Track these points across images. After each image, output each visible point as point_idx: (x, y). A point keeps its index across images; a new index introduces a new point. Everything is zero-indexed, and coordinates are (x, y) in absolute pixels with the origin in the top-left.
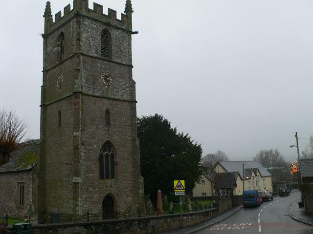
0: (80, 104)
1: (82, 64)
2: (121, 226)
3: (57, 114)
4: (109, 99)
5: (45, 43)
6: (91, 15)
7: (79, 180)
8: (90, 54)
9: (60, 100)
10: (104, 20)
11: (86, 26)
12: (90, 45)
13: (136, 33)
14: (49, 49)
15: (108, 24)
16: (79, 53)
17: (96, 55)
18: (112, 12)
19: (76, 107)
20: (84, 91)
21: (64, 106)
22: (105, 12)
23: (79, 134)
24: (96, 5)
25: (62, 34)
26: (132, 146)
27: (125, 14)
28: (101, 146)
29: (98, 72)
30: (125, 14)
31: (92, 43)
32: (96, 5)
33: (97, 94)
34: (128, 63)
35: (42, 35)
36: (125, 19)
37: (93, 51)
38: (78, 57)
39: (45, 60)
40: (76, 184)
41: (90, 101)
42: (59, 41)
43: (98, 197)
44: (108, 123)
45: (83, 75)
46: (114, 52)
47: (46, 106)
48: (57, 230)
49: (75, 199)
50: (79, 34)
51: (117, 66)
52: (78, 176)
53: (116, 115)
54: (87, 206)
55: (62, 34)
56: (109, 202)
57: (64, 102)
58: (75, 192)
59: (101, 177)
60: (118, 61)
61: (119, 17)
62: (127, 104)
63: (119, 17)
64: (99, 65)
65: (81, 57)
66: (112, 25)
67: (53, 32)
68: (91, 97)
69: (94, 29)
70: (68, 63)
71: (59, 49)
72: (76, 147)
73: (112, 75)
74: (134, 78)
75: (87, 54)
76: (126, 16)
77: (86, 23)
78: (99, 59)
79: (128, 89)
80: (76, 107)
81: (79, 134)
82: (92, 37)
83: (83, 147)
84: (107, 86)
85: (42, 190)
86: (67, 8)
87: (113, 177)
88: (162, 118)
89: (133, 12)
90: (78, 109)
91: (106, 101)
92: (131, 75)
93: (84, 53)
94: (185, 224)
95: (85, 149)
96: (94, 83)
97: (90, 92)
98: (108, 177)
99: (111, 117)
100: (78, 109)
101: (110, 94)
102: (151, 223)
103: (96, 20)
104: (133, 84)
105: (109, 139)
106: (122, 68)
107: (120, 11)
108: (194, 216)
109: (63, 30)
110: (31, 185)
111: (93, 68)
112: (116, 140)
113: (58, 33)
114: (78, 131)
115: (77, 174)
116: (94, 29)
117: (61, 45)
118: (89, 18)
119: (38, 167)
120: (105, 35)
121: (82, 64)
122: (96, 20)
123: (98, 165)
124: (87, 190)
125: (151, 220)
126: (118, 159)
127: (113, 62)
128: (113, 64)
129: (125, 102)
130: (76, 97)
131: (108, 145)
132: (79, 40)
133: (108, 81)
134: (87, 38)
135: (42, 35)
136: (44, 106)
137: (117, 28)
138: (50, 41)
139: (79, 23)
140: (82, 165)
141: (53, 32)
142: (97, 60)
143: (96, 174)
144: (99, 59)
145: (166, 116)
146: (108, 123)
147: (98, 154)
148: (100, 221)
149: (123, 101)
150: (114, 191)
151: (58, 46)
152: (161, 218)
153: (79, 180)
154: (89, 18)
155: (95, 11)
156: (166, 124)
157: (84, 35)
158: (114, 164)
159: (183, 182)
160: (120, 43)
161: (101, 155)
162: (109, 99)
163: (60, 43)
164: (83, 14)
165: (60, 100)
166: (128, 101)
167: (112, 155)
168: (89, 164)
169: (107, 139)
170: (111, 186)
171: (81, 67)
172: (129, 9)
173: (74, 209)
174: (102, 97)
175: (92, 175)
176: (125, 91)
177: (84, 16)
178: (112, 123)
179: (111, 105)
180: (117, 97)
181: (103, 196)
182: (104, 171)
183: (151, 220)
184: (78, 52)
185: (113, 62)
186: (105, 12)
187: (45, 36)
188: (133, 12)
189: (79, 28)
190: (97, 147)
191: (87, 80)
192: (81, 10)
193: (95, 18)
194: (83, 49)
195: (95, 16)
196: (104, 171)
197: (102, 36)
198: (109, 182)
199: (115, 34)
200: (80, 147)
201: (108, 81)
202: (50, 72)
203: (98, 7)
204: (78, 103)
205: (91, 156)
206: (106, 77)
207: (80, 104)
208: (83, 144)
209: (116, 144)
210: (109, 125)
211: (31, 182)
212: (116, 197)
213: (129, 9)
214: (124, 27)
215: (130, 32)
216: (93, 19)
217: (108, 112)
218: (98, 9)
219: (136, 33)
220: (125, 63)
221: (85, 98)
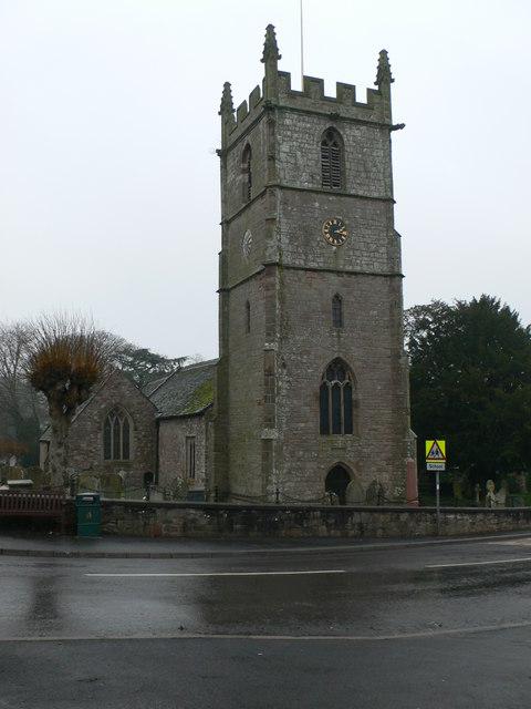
0: (278, 287)
1: (279, 207)
2: (283, 517)
3: (244, 308)
4: (339, 273)
5: (224, 167)
6: (298, 104)
7: (274, 434)
8: (298, 185)
9: (248, 280)
10: (327, 110)
11: (287, 128)
12: (296, 167)
13: (401, 126)
14: (230, 178)
15: (335, 117)
16: (275, 186)
17: (310, 186)
18: (346, 90)
19: (270, 293)
20: (287, 260)
21: (254, 292)
22: (330, 91)
23: (275, 346)
24: (308, 81)
25: (248, 147)
26: (394, 368)
27: (376, 88)
28: (322, 369)
29: (316, 219)
30: (376, 88)
31: (301, 162)
32: (308, 81)
33: (313, 265)
34: (383, 195)
35: (218, 151)
36: (377, 99)
37: (305, 177)
38: (273, 194)
39: (224, 201)
40: (267, 442)
41: (300, 279)
42: (244, 162)
43: (317, 469)
44: (339, 322)
45: (284, 228)
46: (350, 174)
47: (228, 291)
48: (154, 512)
49: (266, 470)
50: (273, 147)
51: (358, 203)
52: (272, 427)
53: (355, 305)
54: (293, 485)
55: (248, 147)
56: (338, 478)
57: (253, 282)
58: (266, 457)
59: (324, 430)
60: (361, 193)
61: (361, 98)
62: (380, 280)
63: (361, 98)
64: (317, 204)
65: (279, 193)
66: (344, 119)
67: (235, 144)
68: (301, 272)
69: (305, 131)
70: (257, 206)
71: (247, 176)
72: (269, 372)
73: (347, 222)
74: (398, 227)
75: (289, 185)
76: (378, 93)
77: (288, 122)
78: (317, 192)
79: (383, 250)
80: (270, 293)
81: (275, 346)
82: (301, 149)
83: (285, 371)
84: (334, 248)
85: (222, 451)
86: (254, 94)
87: (349, 430)
88: (498, 303)
89: (393, 81)
90: (272, 297)
91: (333, 278)
92: (391, 219)
93: (284, 183)
94: (452, 530)
95: (289, 374)
96: (307, 244)
97: (299, 262)
98: (336, 431)
99: (345, 309)
100: (272, 297)
101: (342, 262)
102: (357, 518)
103: (308, 113)
104: (394, 240)
105: (341, 355)
106: (370, 206)
107: (364, 82)
108: (480, 517)
109: (248, 139)
110: (203, 443)
111: (304, 212)
112: (356, 356)
113: (241, 147)
114: (272, 341)
115: (269, 422)
116: (305, 131)
117: (247, 171)
118: (292, 110)
119: (215, 408)
120: (331, 139)
121: (279, 207)
122: (308, 113)
123: (316, 406)
124: (292, 454)
125: (356, 514)
126: (358, 395)
127: (350, 196)
128: (348, 199)
129: (378, 278)
130: (270, 274)
131: (338, 367)
132: (272, 158)
133: (338, 237)
134: (291, 154)
135: (218, 151)
136: (224, 291)
137: (358, 122)
138: (231, 163)
139: (271, 124)
140: (281, 406)
141: (235, 144)
142: (314, 195)
143: (314, 423)
144: (317, 192)
145: (507, 298)
146: (339, 322)
147: (317, 386)
148: (270, 505)
149: (373, 274)
150: (349, 459)
151: (244, 171)
152: (384, 511)
153: (274, 434)
154: (292, 110)
155: (306, 94)
156: (509, 318)
157: (285, 148)
158: (351, 405)
159: (442, 444)
160: (364, 154)
161: (324, 387)
162: (339, 273)
163: (246, 166)
164: (281, 104)
165: (248, 280)
166: (385, 276)
167: (348, 388)
168: (299, 405)
169: (336, 356)
170: (342, 448)
171: (278, 214)
172: (384, 75)
173: (264, 487)
174: (324, 271)
175: (303, 425)
176: (377, 255)
177: (286, 108)
178: (346, 322)
179: (344, 286)
180: (358, 269)
181: (325, 468)
182: (331, 417)
183: (356, 514)
184: (271, 183)
185: (350, 196)
186: (330, 91)
187: (223, 154)
188: (393, 81)
189: (273, 134)
190: (314, 372)
191: (292, 238)
192: (277, 97)
193: (307, 108)
194: (282, 175)
195: (308, 104)
196: (331, 417)
197: (324, 143)
198: (340, 440)
199: (351, 135)
200: (277, 370)
201: (338, 237)
202: (233, 224)
203: (314, 84)
204: (273, 285)
205: (301, 388)
206: (334, 228)
207: (278, 287)
208: (284, 366)
209: (355, 365)
210: (341, 326)
211: (204, 436)
212: (354, 470)
213: (384, 75)
214: (373, 118)
215: (387, 127)
216: (303, 111)
217: (337, 299)
218: (314, 88)
219: (401, 126)
220: (376, 195)
221: (289, 275)
